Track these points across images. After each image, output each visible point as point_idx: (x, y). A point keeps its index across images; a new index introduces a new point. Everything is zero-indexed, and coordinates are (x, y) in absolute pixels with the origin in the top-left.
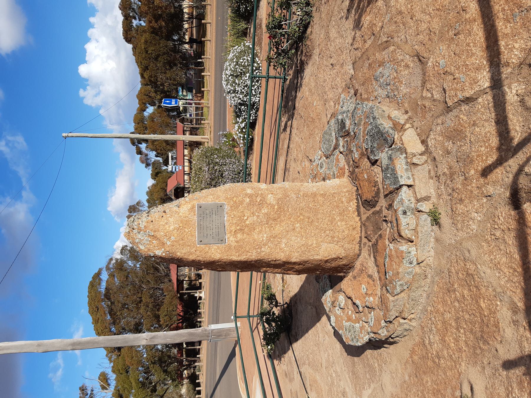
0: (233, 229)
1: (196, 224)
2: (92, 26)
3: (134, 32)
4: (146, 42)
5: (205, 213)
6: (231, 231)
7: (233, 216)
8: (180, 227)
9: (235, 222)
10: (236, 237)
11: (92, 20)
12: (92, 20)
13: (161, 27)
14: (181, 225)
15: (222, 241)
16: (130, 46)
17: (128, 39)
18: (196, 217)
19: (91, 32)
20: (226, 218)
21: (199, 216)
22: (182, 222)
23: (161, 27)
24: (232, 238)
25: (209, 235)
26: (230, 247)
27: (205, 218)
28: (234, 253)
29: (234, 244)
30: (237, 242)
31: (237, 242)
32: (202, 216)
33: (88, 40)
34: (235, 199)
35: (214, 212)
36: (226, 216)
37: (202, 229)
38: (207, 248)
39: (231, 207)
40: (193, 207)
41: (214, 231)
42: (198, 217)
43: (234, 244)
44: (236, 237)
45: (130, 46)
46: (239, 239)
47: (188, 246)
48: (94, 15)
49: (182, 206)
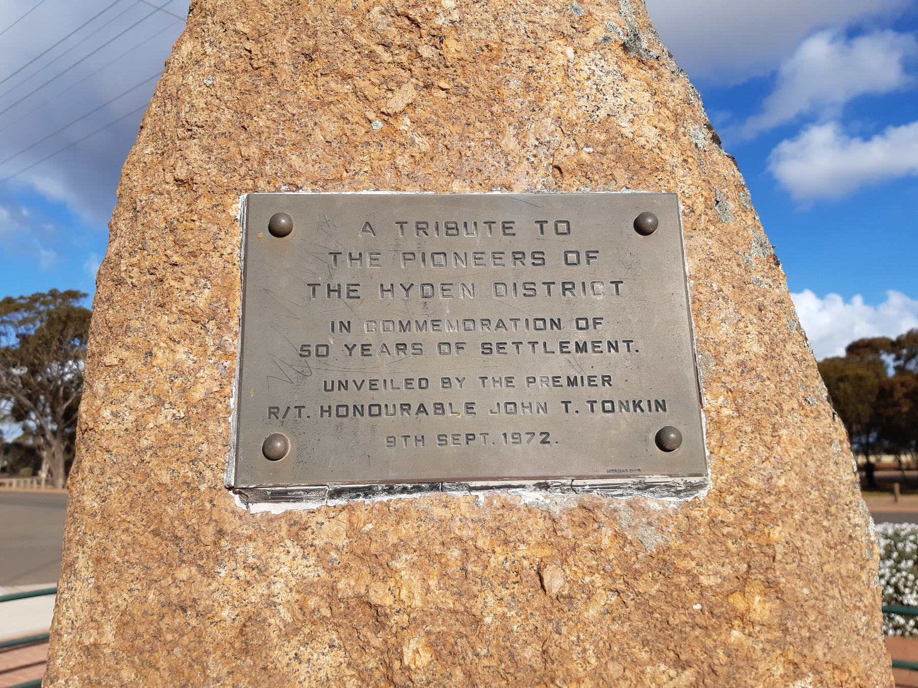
0: (410, 588)
1: (458, 187)
2: (847, 300)
3: (870, 357)
4: (860, 378)
5: (579, 274)
6: (379, 564)
7: (555, 581)
8: (438, 39)
9: (490, 606)
10: (305, 623)
11: (858, 300)
12: (858, 300)
13: (896, 404)
14: (452, 47)
15: (268, 466)
16: (842, 353)
17: (854, 349)
18: (540, 180)
19: (836, 300)
20: (531, 496)
21: (552, 219)
22: (489, 52)
23: (896, 404)
24: (291, 566)
25: (341, 309)
26: (202, 547)
27: (528, 271)
28: (119, 599)
29: (225, 594)
30: (248, 637)
31: (248, 637)
32: (554, 246)
33: (821, 294)
34: (760, 607)
35: (593, 363)
36: (558, 502)
37: (411, 241)
38: (202, 299)
39: (663, 564)
40: (637, 163)
41: (381, 365)
42: (532, 202)
43: (225, 594)
44: (305, 623)
45: (842, 353)
46: (281, 656)
47: (243, 114)
48: (866, 302)
49: (638, 77)
